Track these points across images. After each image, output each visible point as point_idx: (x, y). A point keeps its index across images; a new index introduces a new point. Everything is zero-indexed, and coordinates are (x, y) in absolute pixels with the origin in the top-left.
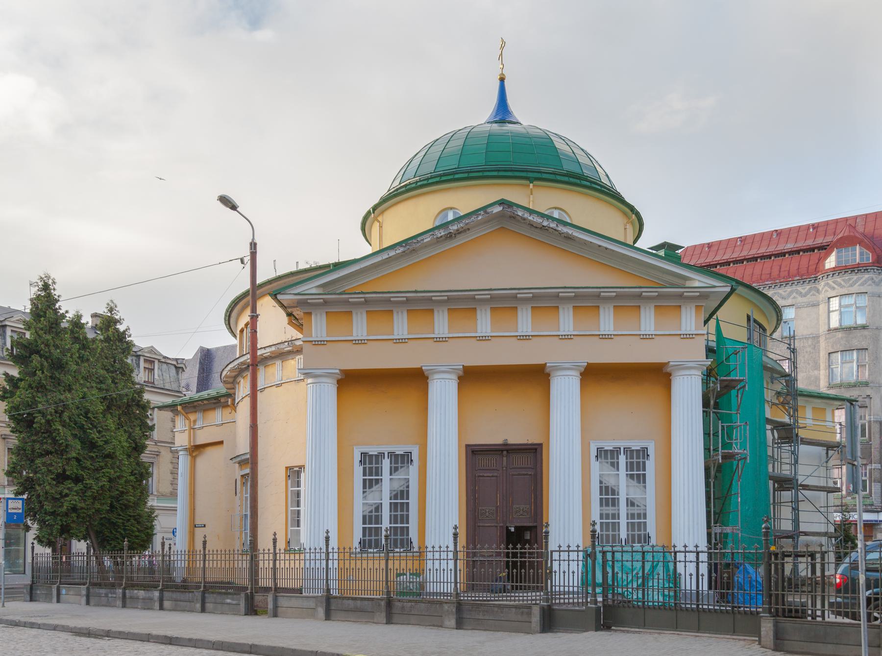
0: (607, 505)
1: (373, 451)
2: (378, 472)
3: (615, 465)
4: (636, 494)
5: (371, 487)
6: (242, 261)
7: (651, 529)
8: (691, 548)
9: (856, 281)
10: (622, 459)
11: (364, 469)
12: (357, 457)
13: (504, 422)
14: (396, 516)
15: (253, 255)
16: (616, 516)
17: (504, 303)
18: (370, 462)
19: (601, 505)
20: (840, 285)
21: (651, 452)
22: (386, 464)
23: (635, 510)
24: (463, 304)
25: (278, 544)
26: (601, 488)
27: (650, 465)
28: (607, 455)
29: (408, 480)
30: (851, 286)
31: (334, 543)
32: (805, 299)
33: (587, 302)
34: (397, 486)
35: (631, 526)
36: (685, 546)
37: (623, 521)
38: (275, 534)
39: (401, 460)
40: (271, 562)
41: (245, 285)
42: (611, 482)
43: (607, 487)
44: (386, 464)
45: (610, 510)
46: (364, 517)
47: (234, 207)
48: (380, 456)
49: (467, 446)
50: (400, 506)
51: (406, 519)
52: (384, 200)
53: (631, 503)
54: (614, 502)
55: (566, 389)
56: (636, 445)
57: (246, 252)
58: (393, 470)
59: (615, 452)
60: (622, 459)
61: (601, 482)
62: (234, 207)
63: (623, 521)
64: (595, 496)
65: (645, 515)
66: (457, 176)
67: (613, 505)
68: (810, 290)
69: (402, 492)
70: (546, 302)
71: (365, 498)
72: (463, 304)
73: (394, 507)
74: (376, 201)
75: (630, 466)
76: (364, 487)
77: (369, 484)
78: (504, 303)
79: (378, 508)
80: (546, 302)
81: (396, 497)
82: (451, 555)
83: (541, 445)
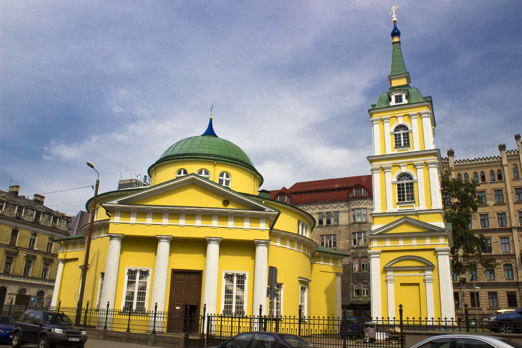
0: (228, 298)
1: (133, 269)
2: (134, 278)
3: (232, 281)
4: (240, 293)
5: (131, 284)
6: (93, 187)
7: (245, 309)
8: (316, 318)
9: (362, 203)
10: (235, 279)
11: (129, 277)
12: (127, 271)
13: (188, 261)
14: (140, 297)
15: (97, 186)
16: (231, 303)
17: (191, 214)
18: (132, 274)
19: (225, 298)
20: (356, 204)
21: (247, 276)
22: (138, 275)
23: (239, 300)
24: (175, 213)
25: (403, 313)
26: (226, 290)
27: (246, 282)
28: (229, 277)
29: (146, 282)
30: (360, 205)
31: (111, 307)
32: (342, 209)
33: (223, 216)
34: (141, 285)
35: (237, 307)
36: (294, 317)
37: (234, 305)
38: (156, 304)
39: (144, 274)
40: (153, 318)
41: (92, 195)
42: (230, 288)
43: (228, 290)
44: (138, 275)
45: (229, 300)
46: (127, 297)
47: (92, 167)
48: (135, 272)
49: (172, 269)
50: (142, 294)
51: (144, 299)
52: (158, 162)
53: (238, 297)
54: (231, 297)
55: (213, 248)
56: (241, 273)
57: (95, 184)
58: (141, 278)
59: (232, 276)
60: (235, 279)
61: (226, 288)
62: (92, 167)
63: (234, 305)
64: (223, 294)
65: (243, 303)
66: (186, 156)
67: (231, 298)
68: (330, 206)
69: (143, 287)
70: (207, 214)
71: (128, 289)
72: (175, 213)
73: (139, 293)
74: (154, 163)
75: (238, 282)
76: (128, 284)
77: (131, 283)
78: (191, 214)
79: (133, 293)
80: (207, 214)
81: (141, 289)
82: (157, 315)
83: (202, 271)
